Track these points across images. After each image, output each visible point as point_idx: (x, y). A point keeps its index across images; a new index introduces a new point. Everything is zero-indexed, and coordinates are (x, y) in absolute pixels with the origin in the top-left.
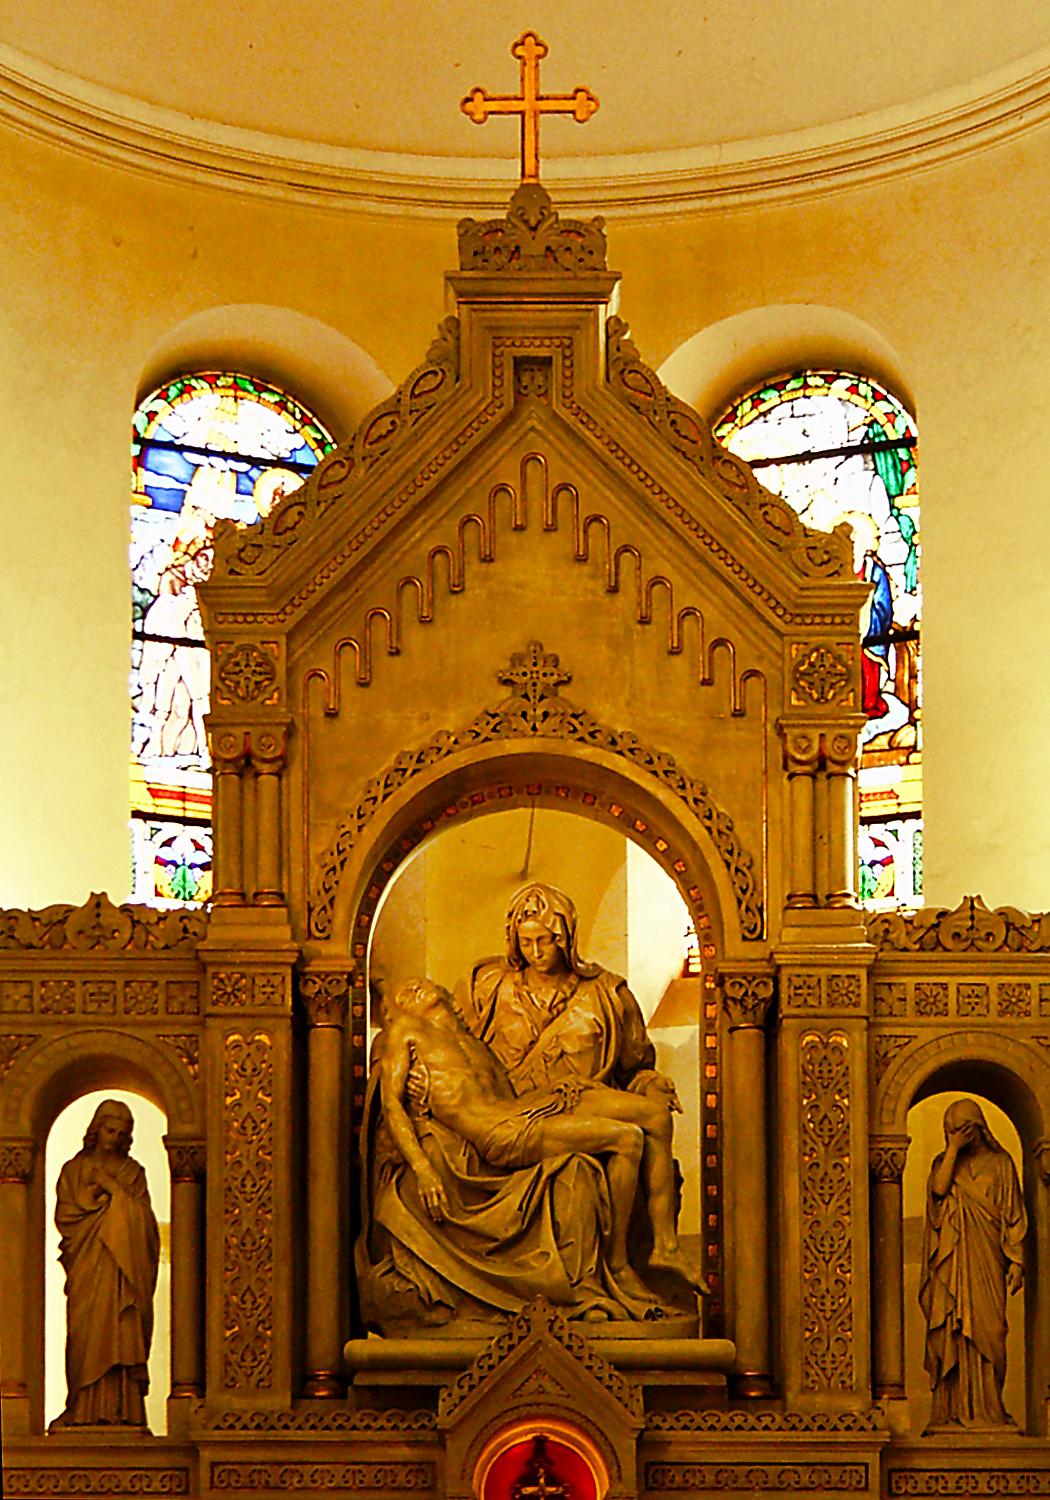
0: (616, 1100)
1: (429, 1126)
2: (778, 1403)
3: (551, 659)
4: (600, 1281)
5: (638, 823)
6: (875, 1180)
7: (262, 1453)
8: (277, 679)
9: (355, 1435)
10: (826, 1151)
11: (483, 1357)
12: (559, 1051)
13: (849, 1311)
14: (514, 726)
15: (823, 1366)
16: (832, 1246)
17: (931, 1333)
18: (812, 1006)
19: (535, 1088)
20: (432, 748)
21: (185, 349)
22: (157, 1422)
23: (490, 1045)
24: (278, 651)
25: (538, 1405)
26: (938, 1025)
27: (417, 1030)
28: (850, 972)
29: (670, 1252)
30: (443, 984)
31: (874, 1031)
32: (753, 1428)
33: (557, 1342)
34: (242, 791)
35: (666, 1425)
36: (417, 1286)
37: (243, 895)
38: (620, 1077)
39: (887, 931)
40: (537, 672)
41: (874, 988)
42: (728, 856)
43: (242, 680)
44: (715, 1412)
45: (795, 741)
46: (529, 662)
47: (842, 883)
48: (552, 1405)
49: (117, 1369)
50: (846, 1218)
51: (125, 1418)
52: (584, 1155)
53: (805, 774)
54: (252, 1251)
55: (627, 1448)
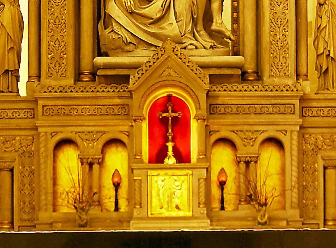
4: (193, 35)
11: (147, 62)
13: (287, 46)
16: (281, 22)
17: (318, 56)
21: (59, 174)
22: (23, 92)
29: (219, 24)
33: (176, 56)
36: (122, 37)
48: (173, 81)
49: (7, 71)
50: (287, 11)
51: (10, 90)
54: (59, 25)
55: (203, 97)
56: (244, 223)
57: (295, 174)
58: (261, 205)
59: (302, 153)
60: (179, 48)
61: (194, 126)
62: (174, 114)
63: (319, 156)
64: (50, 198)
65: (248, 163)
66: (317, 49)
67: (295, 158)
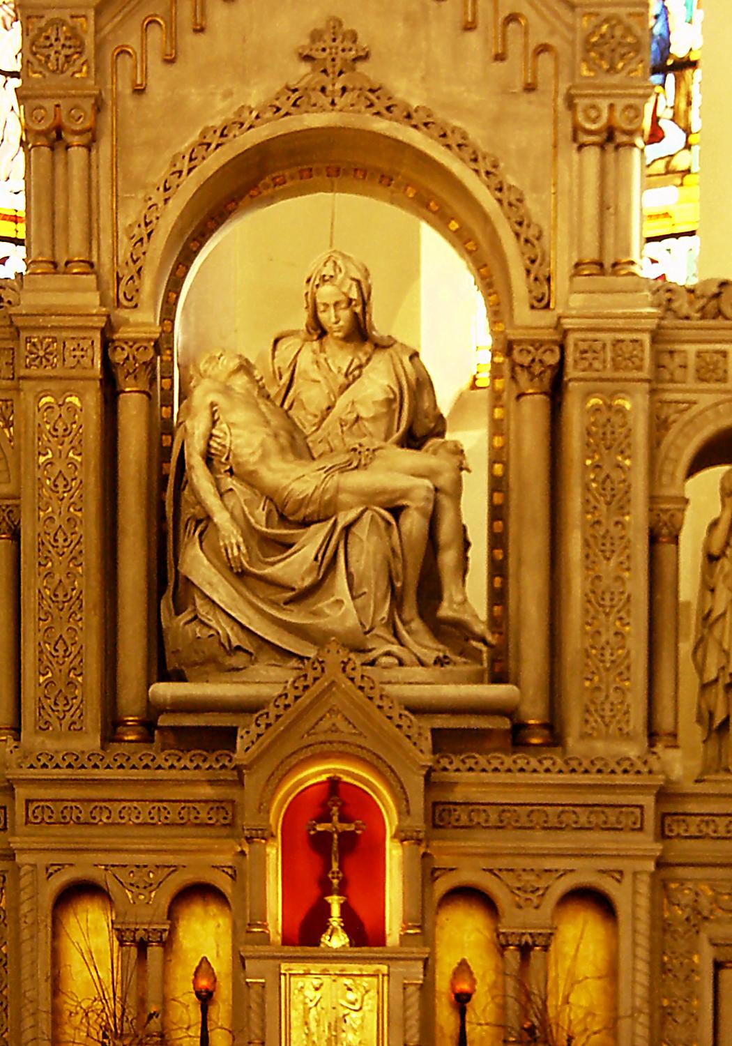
0: (410, 458)
1: (229, 482)
2: (559, 749)
3: (349, 36)
5: (432, 204)
6: (653, 539)
7: (74, 790)
8: (86, 52)
9: (160, 774)
10: (608, 510)
11: (280, 696)
12: (355, 415)
14: (313, 101)
15: (602, 713)
16: (612, 600)
17: (705, 687)
18: (597, 371)
19: (332, 451)
20: (234, 123)
23: (291, 412)
24: (87, 27)
25: (331, 743)
26: (718, 391)
27: (218, 391)
28: (635, 336)
30: (246, 356)
31: (656, 398)
32: (535, 771)
33: (349, 683)
34: (53, 164)
35: (454, 767)
36: (218, 633)
37: (55, 264)
38: (412, 440)
39: (670, 300)
40: (337, 48)
41: (656, 355)
42: (517, 227)
43: (52, 54)
44: (499, 755)
45: (585, 111)
46: (328, 37)
47: (627, 252)
52: (377, 509)
53: (593, 144)
54: (64, 602)
55: (415, 784)
57: (642, 978)
59: (661, 928)
60: (358, 663)
61: (394, 854)
63: (704, 936)
64: (45, 1026)
65: (525, 950)
66: (701, 670)
67: (643, 941)
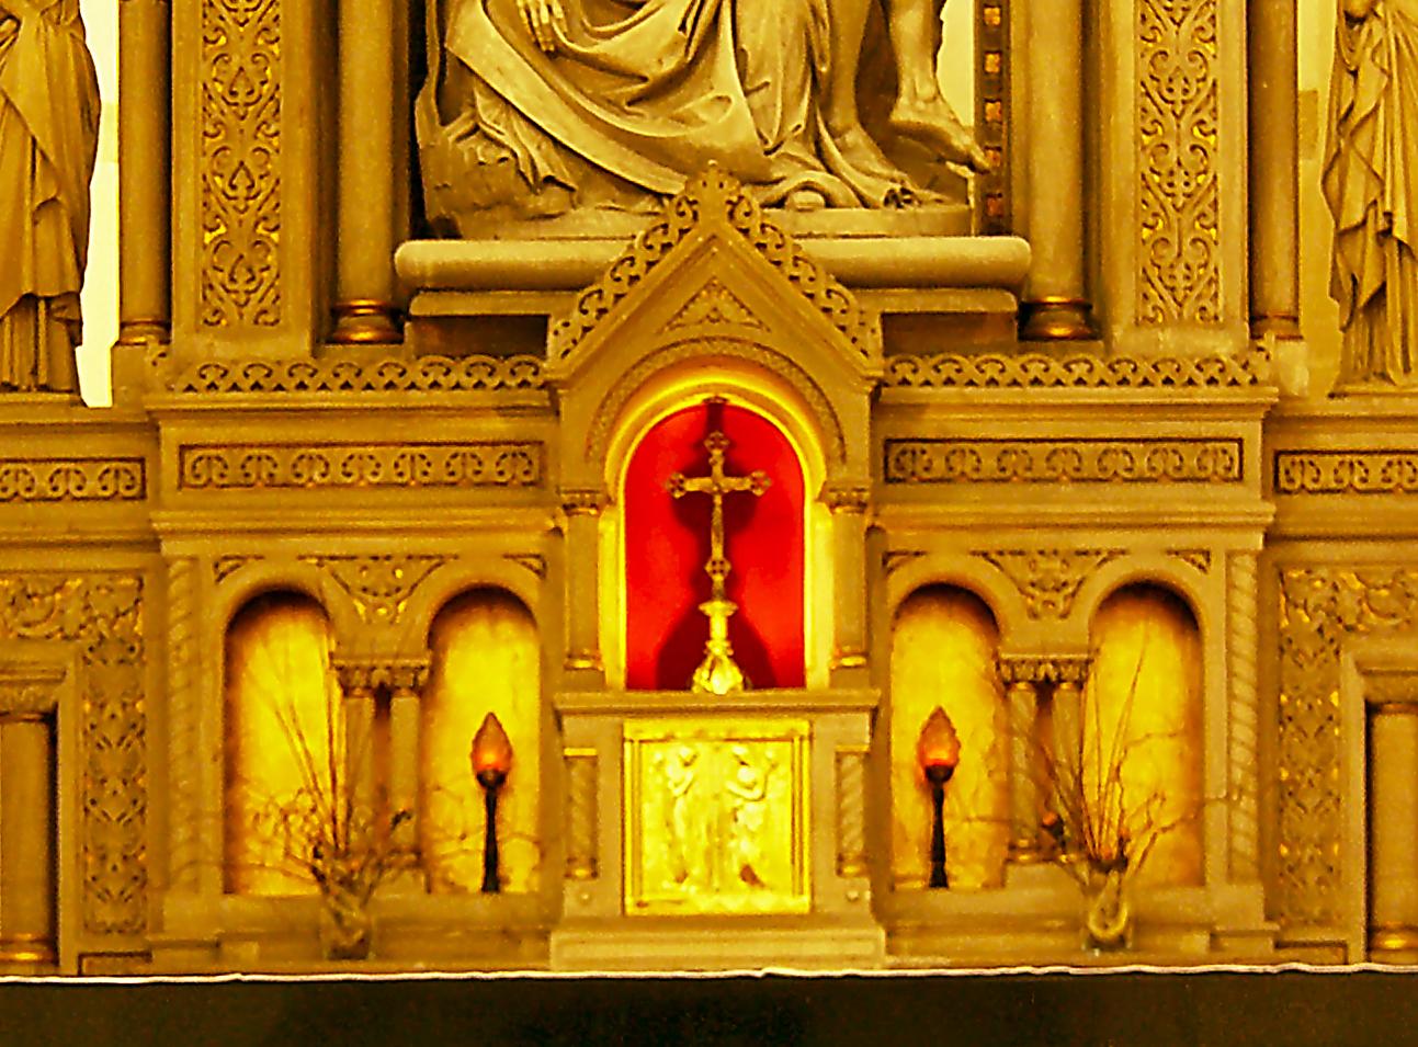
4: (813, 148)
13: (1212, 195)
17: (1342, 236)
22: (97, 389)
29: (926, 102)
33: (741, 238)
36: (515, 155)
48: (732, 340)
49: (29, 301)
50: (1209, 47)
51: (43, 381)
54: (247, 105)
55: (855, 408)
56: (1031, 940)
57: (1244, 733)
58: (1100, 865)
59: (1275, 645)
60: (756, 203)
61: (820, 531)
62: (734, 483)
63: (1347, 659)
64: (211, 837)
65: (1045, 690)
66: (1336, 206)
67: (1245, 669)
